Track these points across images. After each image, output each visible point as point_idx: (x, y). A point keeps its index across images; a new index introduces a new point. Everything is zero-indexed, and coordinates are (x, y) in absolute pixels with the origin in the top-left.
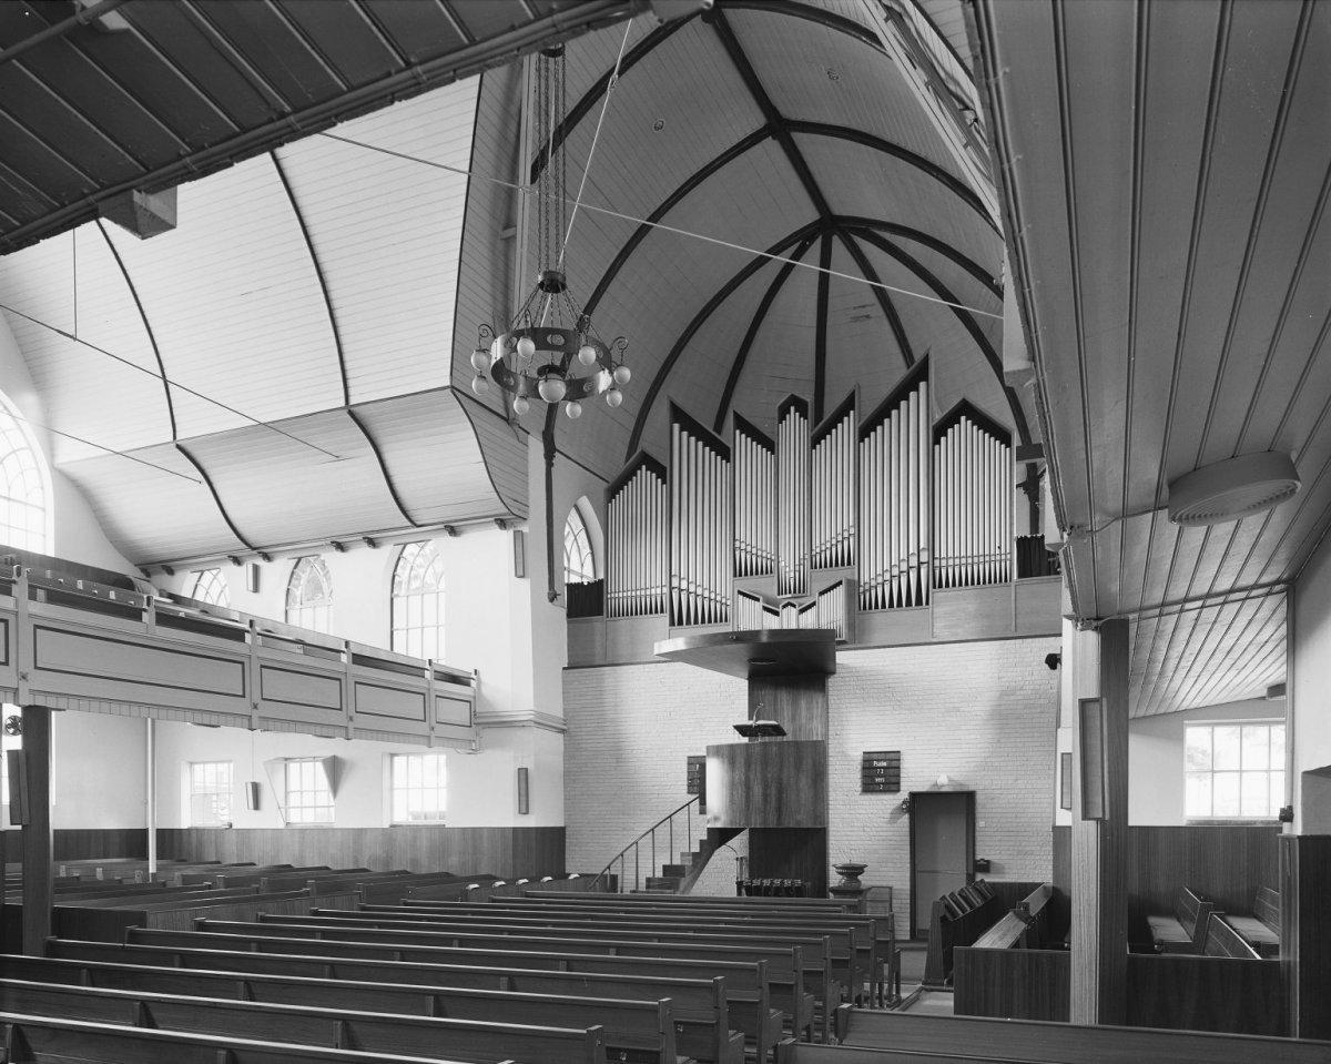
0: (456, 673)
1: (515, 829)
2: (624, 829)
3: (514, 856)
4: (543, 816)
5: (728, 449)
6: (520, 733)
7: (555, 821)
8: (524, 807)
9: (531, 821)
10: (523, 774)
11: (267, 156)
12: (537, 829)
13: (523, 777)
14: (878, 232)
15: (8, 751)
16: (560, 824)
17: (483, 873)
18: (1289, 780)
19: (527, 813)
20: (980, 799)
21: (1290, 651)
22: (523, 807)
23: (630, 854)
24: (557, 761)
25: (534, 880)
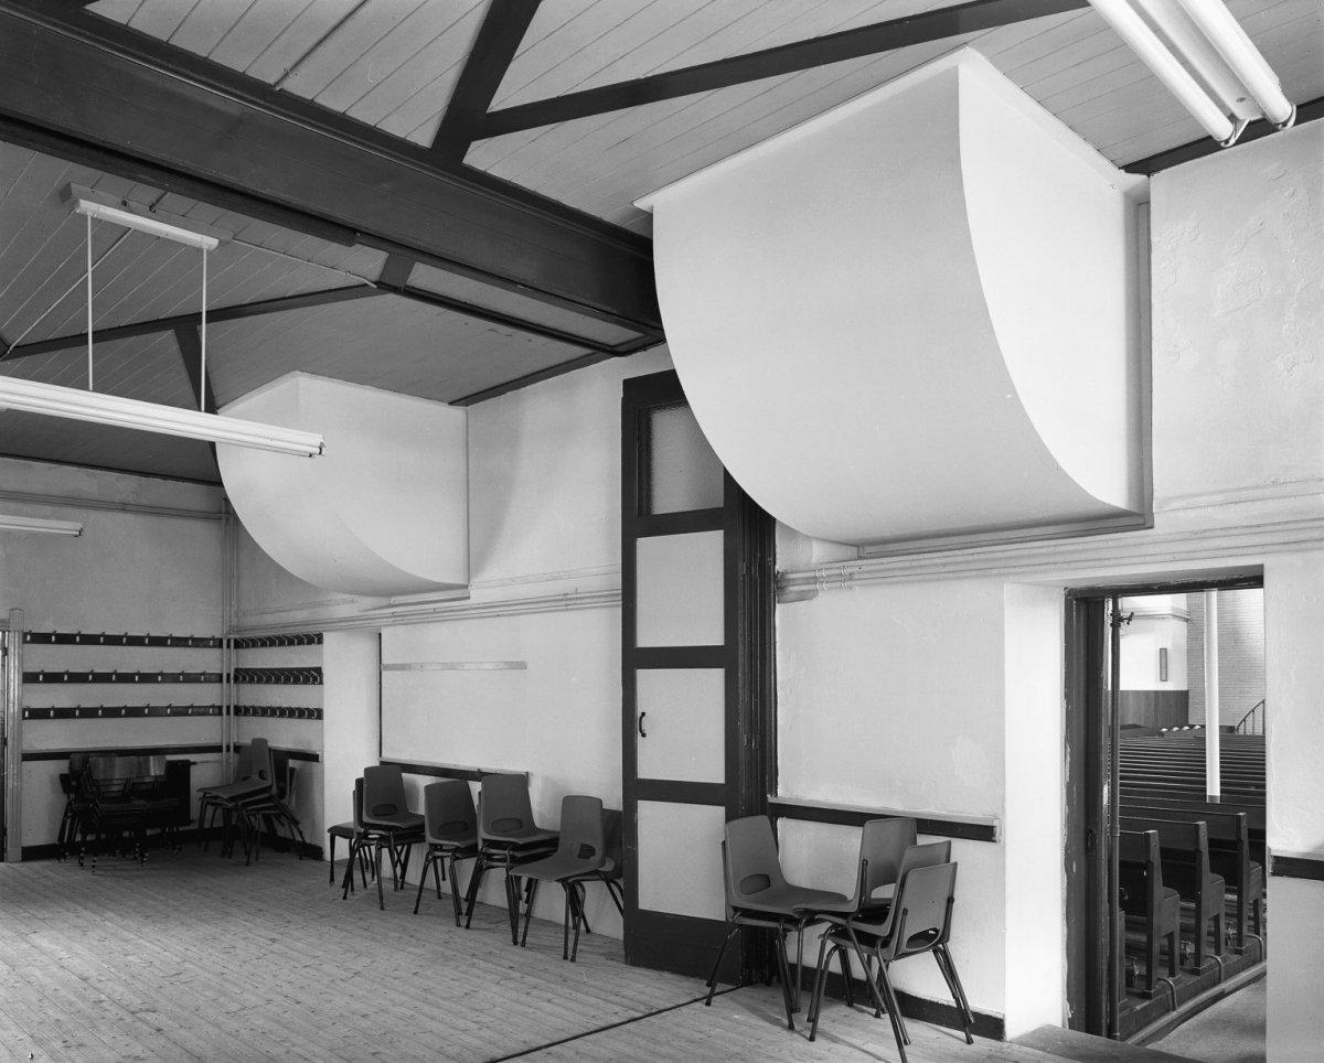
0: (1147, 582)
1: (1156, 692)
2: (1241, 692)
3: (1156, 711)
4: (1174, 684)
5: (1123, 905)
6: (1158, 624)
7: (1184, 687)
8: (1164, 677)
9: (1169, 686)
10: (1163, 652)
11: (714, 636)
12: (1174, 692)
13: (1163, 654)
14: (450, 780)
15: (1262, 566)
16: (1186, 689)
17: (1130, 723)
18: (474, 274)
19: (1166, 680)
20: (316, 687)
21: (1146, 494)
22: (1164, 676)
23: (1259, 711)
24: (1183, 641)
25: (1170, 729)
